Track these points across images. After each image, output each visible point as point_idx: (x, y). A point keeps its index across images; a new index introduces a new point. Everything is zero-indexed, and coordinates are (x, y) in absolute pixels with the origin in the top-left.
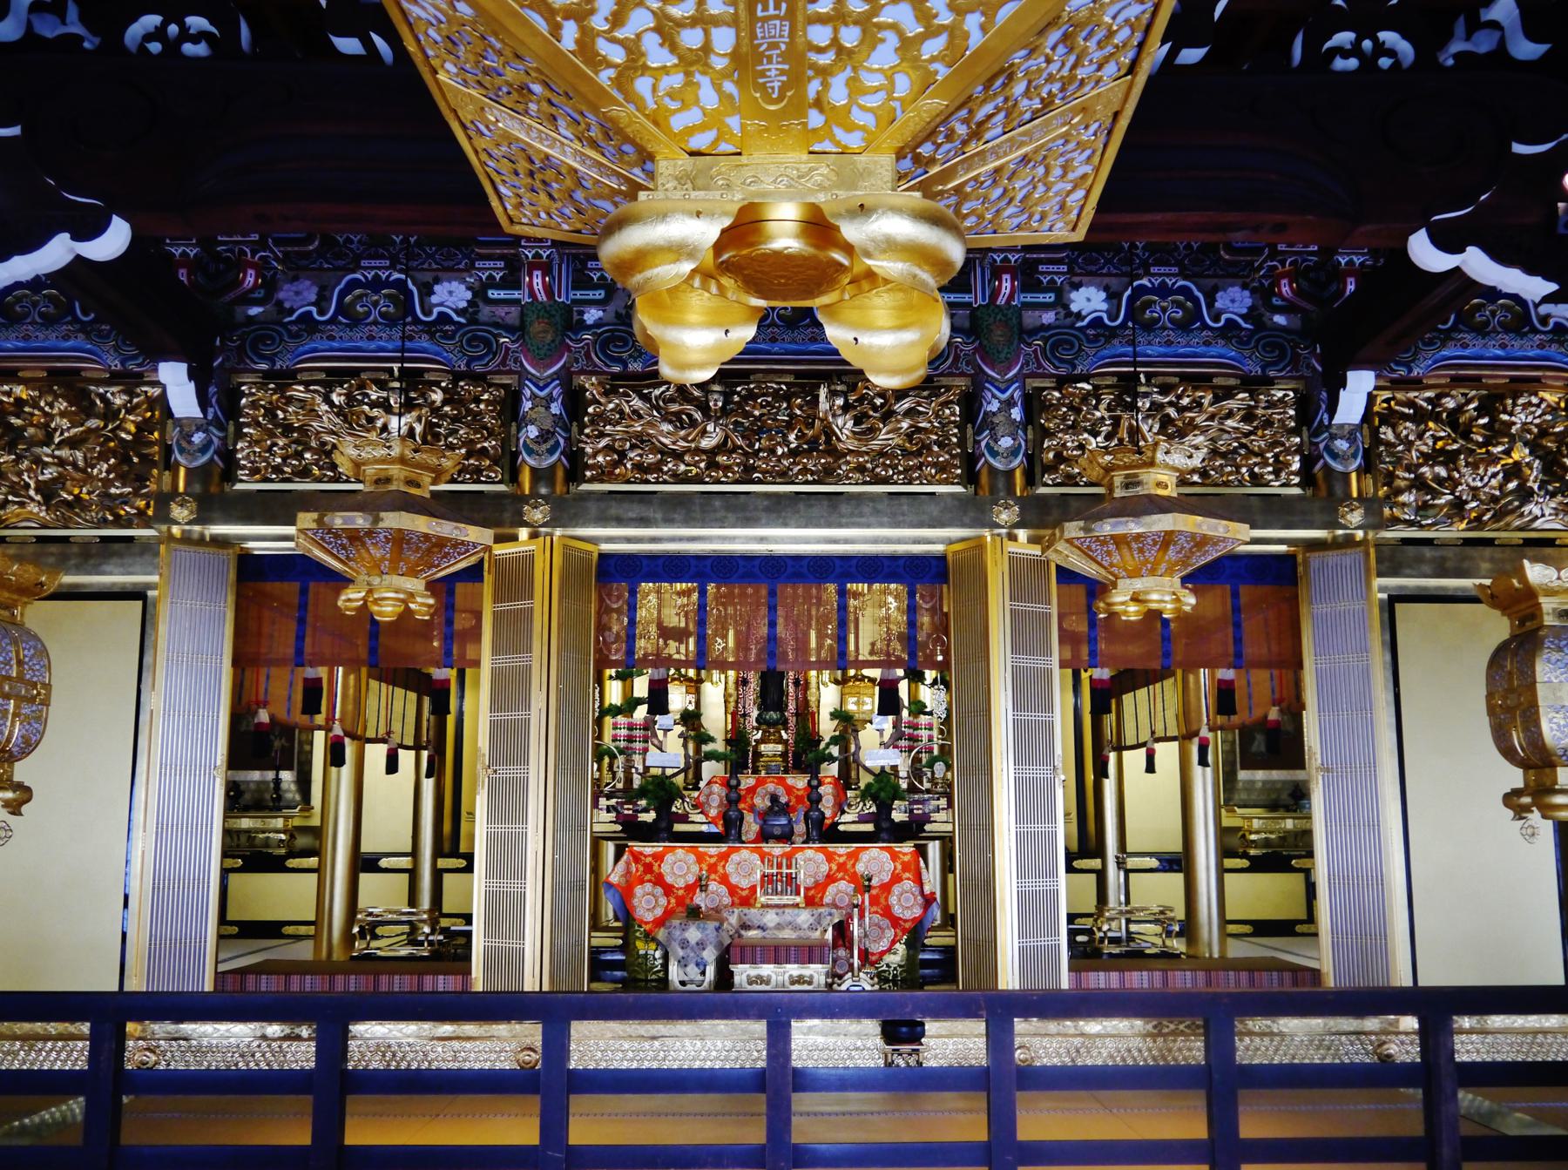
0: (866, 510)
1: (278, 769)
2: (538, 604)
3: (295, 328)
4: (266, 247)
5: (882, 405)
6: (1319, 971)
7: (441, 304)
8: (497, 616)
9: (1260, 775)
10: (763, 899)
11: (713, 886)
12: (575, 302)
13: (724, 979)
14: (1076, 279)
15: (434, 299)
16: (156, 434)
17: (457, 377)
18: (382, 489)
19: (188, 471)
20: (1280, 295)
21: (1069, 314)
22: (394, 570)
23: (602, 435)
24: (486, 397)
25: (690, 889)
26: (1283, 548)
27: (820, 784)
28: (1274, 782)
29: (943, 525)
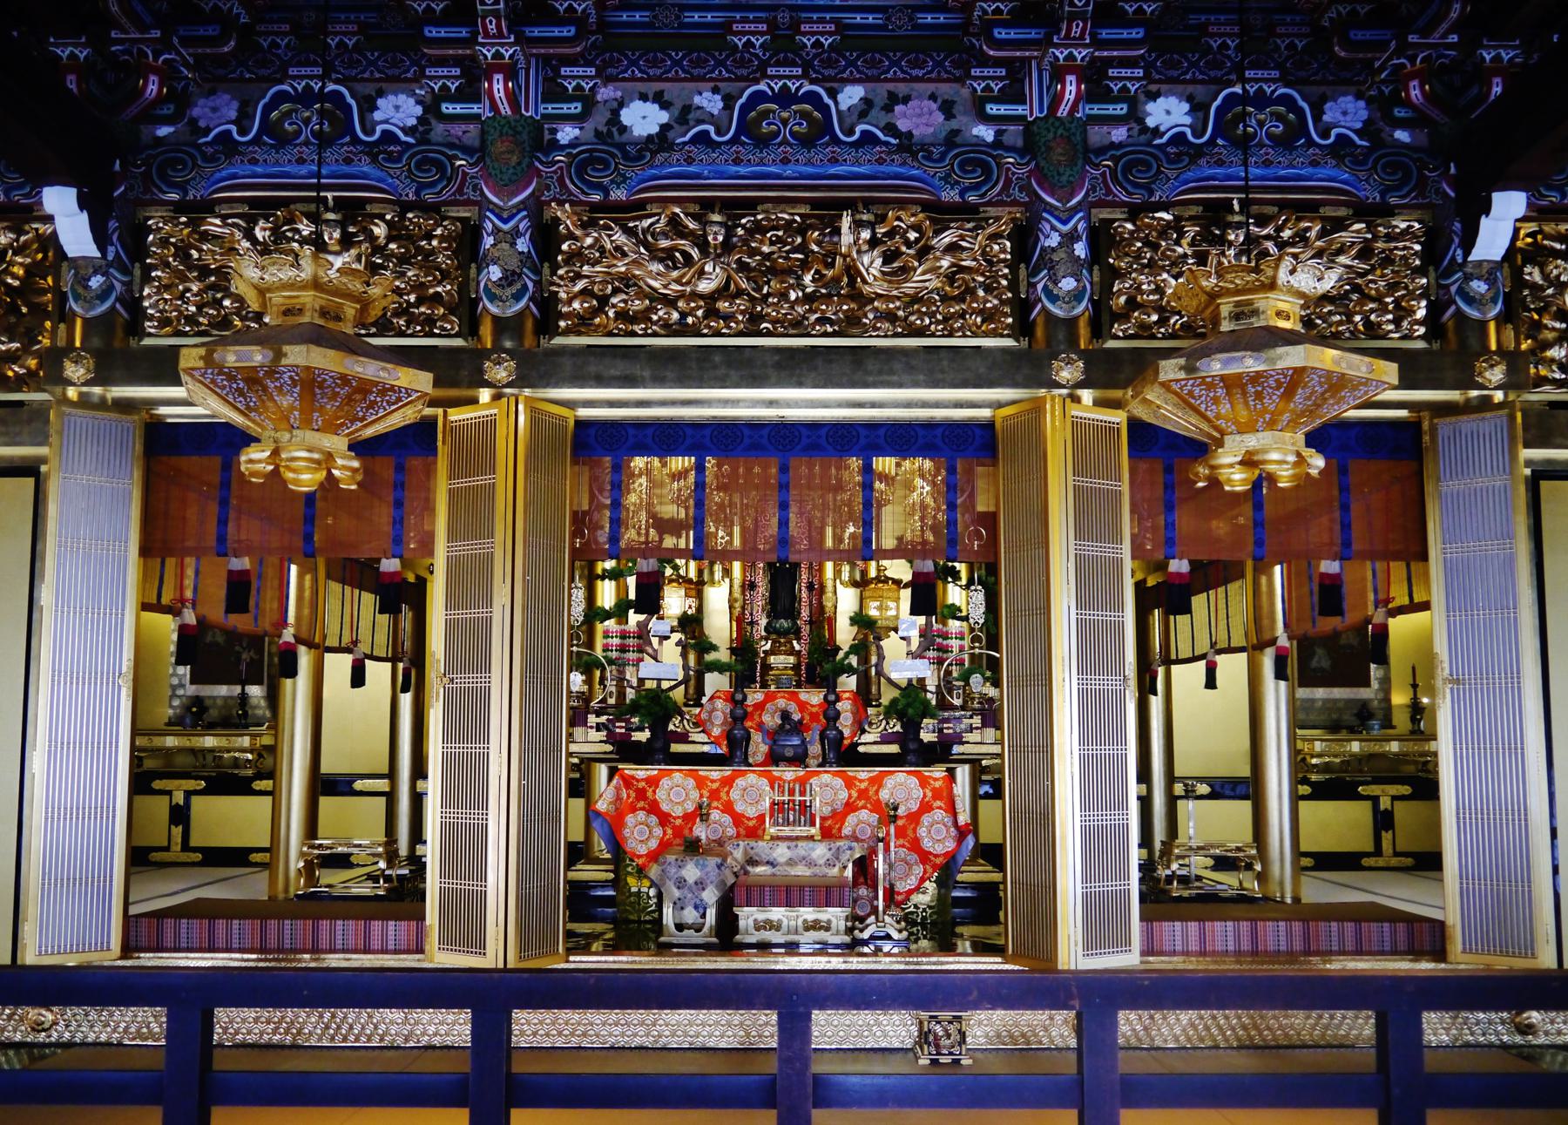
0: (897, 366)
1: (243, 683)
2: (501, 480)
3: (210, 150)
4: (170, 48)
5: (917, 240)
6: (1442, 924)
7: (386, 122)
8: (452, 493)
9: (1320, 693)
10: (773, 831)
11: (715, 815)
13: (727, 923)
14: (1154, 88)
15: (377, 116)
16: (50, 280)
17: (405, 207)
18: (292, 320)
19: (86, 321)
20: (1407, 103)
21: (1145, 129)
22: (307, 423)
23: (579, 276)
24: (439, 232)
25: (689, 818)
26: (1403, 413)
27: (838, 699)
28: (1335, 701)
29: (990, 385)
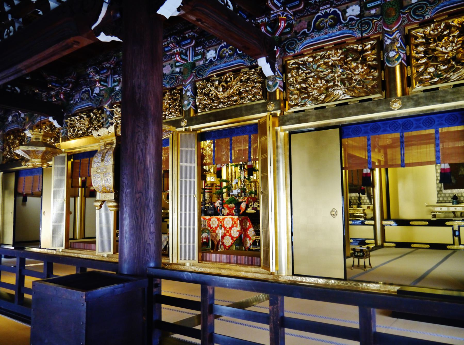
12: (195, 61)
15: (347, 15)
